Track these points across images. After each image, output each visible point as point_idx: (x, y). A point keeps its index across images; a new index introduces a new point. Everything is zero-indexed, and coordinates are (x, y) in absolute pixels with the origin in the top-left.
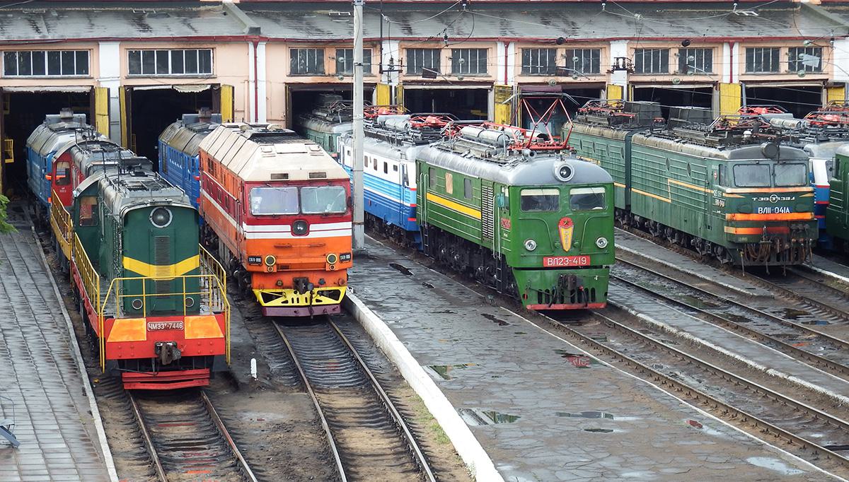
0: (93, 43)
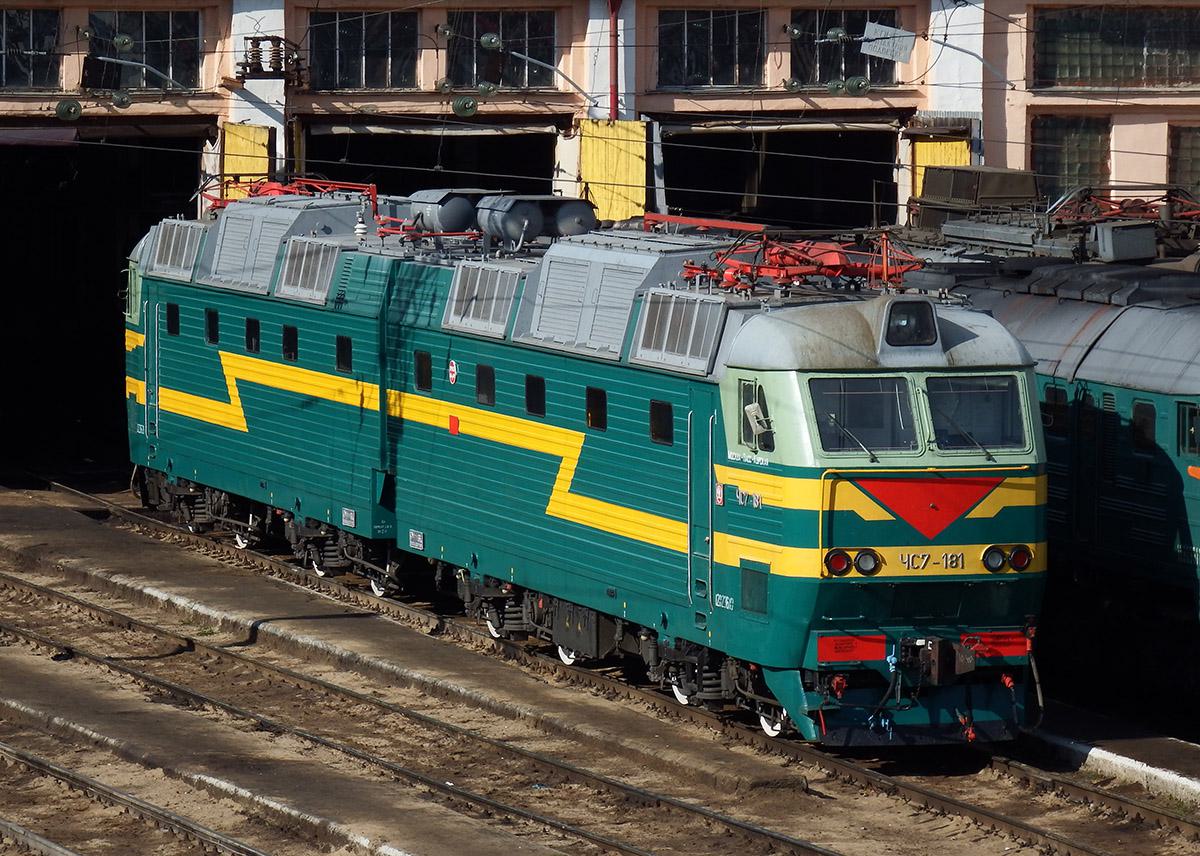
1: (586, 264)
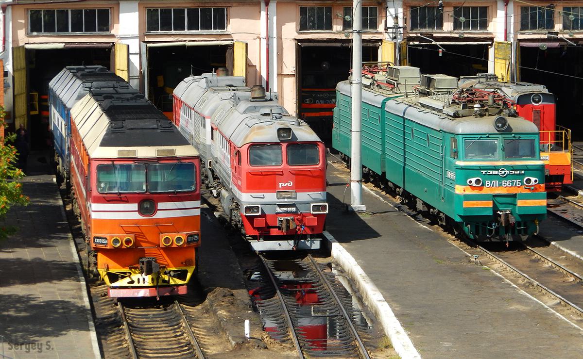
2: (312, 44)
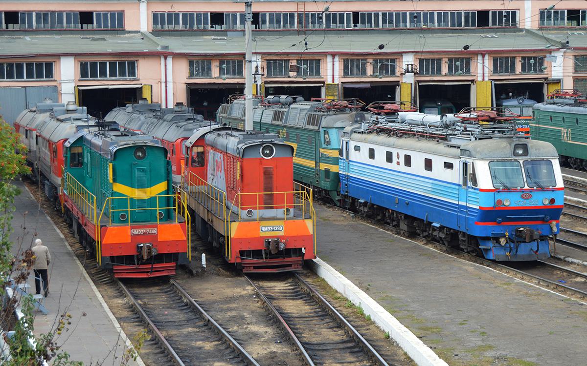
0: (57, 57)
1: (297, 109)
2: (460, 83)
